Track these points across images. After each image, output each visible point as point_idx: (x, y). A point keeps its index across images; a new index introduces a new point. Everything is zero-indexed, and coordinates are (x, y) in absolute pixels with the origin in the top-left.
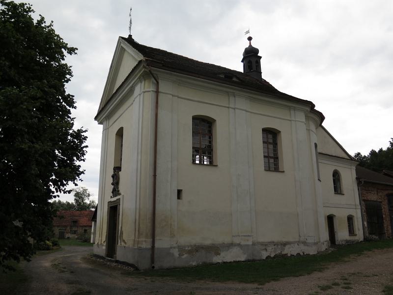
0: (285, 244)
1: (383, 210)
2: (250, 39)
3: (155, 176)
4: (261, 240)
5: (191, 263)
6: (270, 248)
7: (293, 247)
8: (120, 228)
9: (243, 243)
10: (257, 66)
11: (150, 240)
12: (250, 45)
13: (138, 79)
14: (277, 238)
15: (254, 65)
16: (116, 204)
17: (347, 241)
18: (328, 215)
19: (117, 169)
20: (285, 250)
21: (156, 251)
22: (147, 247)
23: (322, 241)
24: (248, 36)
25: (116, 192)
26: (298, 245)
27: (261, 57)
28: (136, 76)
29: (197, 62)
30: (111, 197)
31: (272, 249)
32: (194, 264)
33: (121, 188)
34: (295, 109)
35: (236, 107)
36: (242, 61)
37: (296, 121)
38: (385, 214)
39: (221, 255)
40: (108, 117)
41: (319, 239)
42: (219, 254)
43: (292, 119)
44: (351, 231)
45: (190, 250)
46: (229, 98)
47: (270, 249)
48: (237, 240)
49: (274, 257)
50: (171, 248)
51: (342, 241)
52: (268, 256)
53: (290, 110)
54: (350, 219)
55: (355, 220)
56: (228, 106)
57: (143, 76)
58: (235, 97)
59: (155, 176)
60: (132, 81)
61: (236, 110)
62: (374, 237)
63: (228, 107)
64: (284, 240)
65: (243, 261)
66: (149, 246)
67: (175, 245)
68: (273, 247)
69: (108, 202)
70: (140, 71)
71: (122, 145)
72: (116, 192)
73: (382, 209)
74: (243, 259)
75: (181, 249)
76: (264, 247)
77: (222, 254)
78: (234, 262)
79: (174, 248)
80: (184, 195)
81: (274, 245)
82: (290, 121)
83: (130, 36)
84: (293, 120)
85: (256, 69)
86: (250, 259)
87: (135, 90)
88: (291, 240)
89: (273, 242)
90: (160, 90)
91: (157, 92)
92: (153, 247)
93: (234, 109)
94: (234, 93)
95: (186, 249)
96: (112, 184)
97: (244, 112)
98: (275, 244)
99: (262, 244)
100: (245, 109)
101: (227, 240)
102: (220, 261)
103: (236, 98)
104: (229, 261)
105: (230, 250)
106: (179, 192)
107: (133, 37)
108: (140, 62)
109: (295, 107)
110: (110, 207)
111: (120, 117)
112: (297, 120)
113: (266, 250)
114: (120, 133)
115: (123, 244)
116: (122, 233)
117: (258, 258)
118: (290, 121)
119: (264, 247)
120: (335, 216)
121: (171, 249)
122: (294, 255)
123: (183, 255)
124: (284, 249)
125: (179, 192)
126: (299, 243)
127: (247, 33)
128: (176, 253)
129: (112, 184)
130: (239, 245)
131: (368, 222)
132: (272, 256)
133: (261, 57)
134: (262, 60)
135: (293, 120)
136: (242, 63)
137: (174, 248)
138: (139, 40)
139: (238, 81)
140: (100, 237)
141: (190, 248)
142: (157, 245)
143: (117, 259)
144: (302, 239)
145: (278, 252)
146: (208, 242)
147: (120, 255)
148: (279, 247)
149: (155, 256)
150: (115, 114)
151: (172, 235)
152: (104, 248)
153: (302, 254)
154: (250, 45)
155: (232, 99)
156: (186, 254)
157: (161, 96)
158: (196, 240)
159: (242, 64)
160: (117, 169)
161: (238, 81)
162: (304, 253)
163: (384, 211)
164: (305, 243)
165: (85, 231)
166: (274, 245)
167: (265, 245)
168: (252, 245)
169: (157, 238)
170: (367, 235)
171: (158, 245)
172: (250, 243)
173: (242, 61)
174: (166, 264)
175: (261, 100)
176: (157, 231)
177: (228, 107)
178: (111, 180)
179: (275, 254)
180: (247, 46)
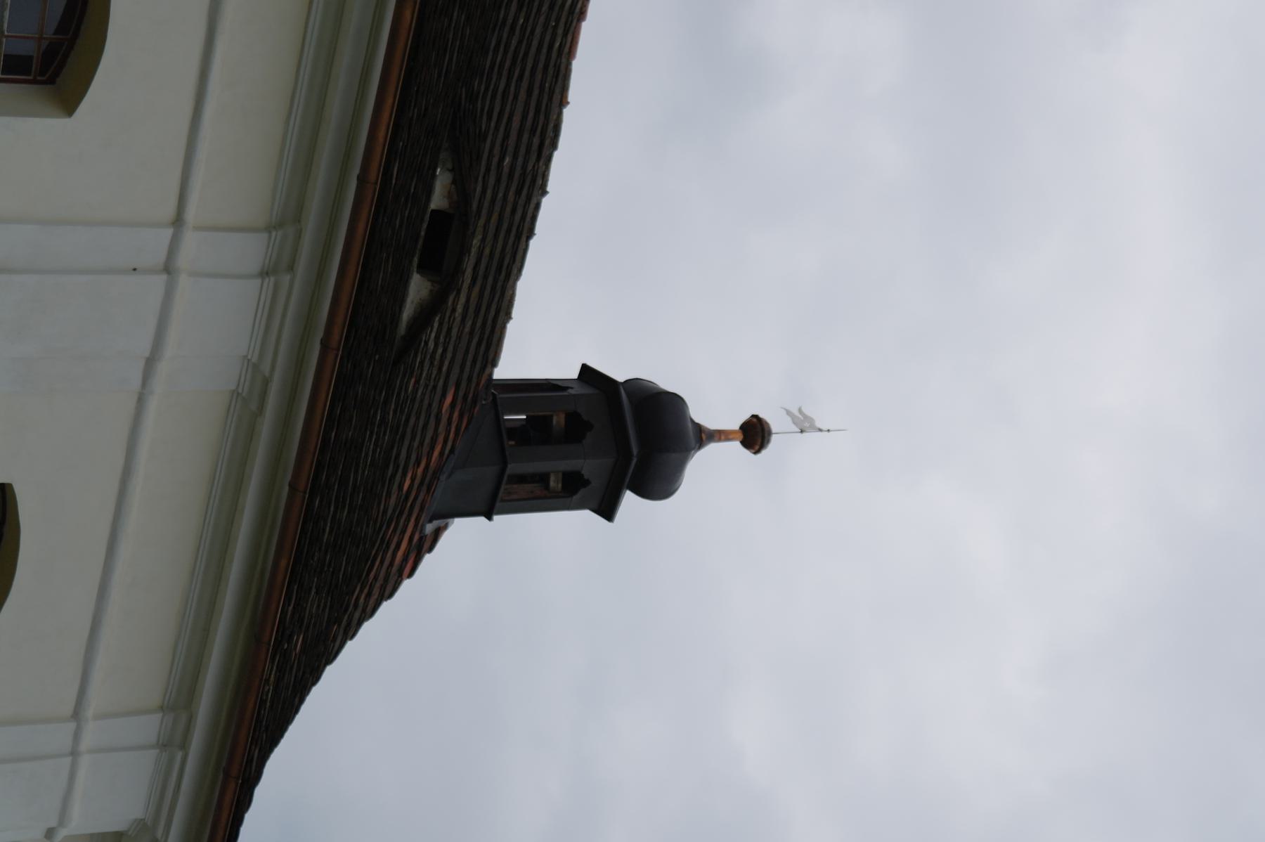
10: (543, 479)
12: (703, 436)
15: (555, 466)
18: (13, 484)
27: (607, 510)
34: (171, 743)
35: (184, 282)
36: (585, 369)
37: (74, 753)
53: (269, 229)
56: (191, 214)
58: (264, 274)
61: (164, 277)
63: (178, 221)
82: (77, 715)
84: (77, 736)
85: (521, 479)
93: (168, 268)
94: (291, 268)
97: (143, 346)
103: (158, 716)
109: (184, 746)
112: (85, 762)
118: (77, 715)
127: (795, 420)
133: (607, 510)
134: (585, 518)
135: (77, 736)
136: (574, 374)
139: (407, 312)
154: (703, 436)
155: (148, 728)
159: (571, 372)
161: (407, 312)
173: (585, 369)
175: (251, 434)
177: (178, 221)
180: (702, 412)
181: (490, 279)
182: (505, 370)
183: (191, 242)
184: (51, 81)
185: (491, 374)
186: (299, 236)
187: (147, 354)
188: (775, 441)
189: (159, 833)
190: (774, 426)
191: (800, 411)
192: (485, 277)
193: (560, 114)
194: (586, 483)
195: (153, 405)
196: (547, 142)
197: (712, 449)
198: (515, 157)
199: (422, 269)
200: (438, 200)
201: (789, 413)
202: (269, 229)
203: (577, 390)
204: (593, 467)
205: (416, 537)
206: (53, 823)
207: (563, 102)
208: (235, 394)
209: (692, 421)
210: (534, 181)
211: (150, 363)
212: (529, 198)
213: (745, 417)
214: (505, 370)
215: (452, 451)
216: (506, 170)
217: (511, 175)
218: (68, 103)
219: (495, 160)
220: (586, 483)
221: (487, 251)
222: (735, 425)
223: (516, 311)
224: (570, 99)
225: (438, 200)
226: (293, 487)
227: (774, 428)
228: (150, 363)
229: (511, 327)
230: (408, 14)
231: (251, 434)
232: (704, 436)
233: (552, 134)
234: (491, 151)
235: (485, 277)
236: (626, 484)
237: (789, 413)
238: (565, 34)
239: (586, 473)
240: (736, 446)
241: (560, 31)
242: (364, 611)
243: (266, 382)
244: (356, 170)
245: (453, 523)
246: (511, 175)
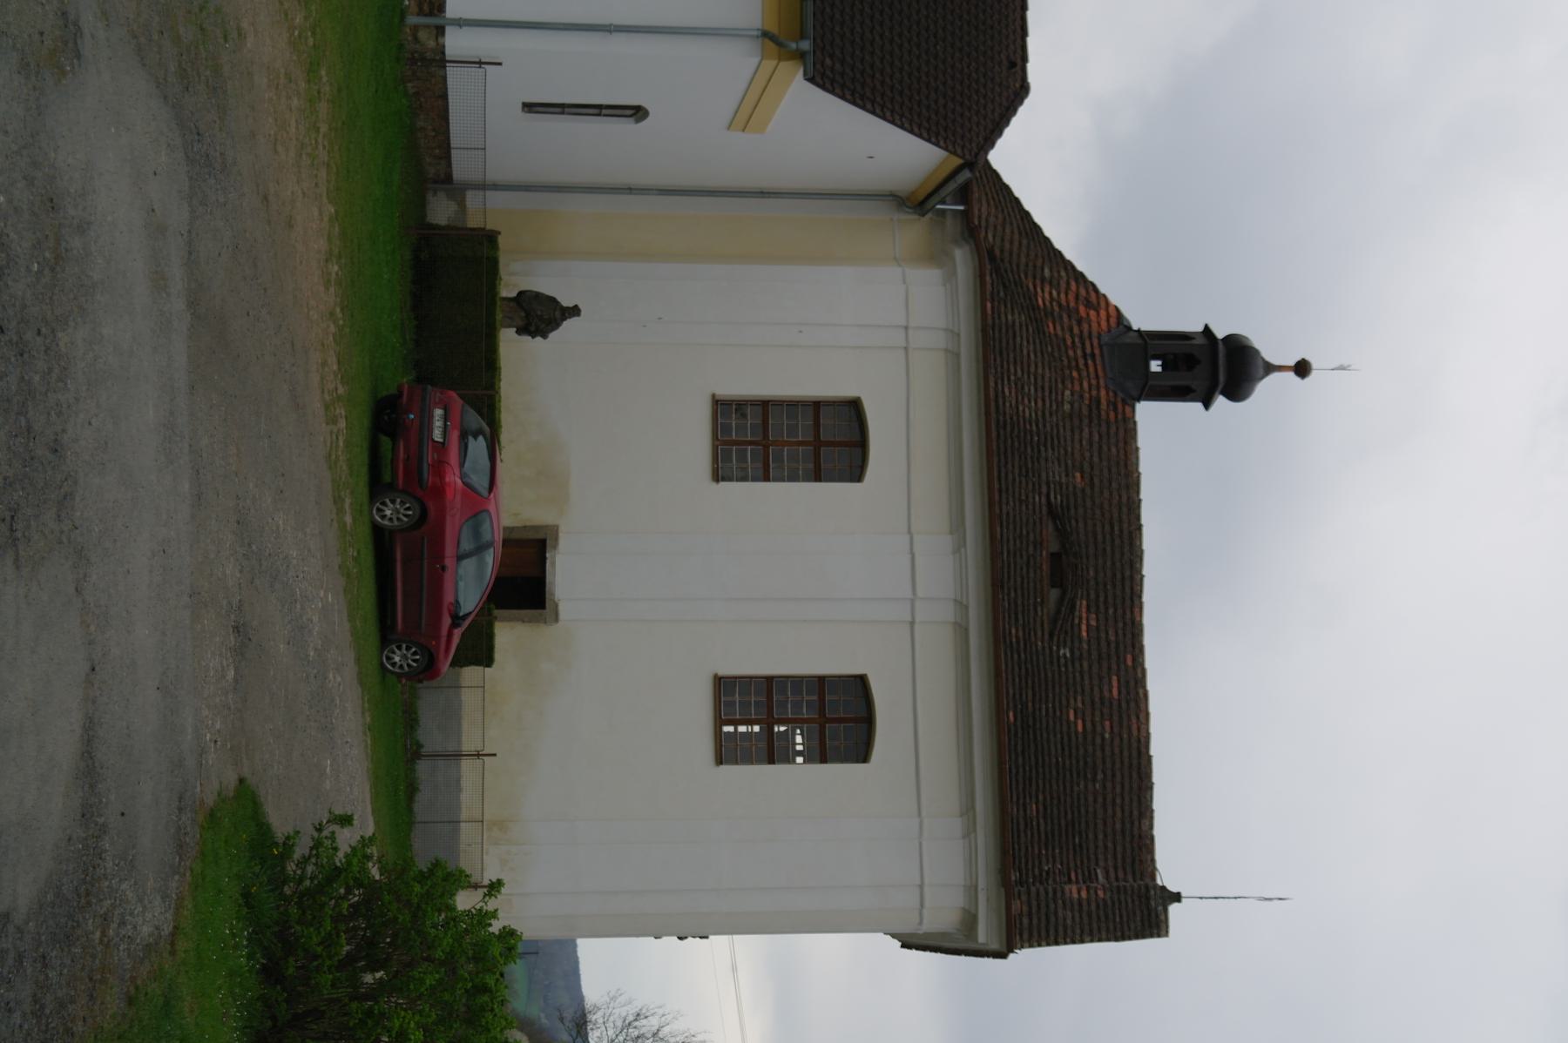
2: (1302, 369)
12: (1270, 368)
27: (1207, 404)
34: (969, 832)
133: (1207, 404)
154: (1270, 368)
155: (956, 825)
188: (1314, 375)
197: (1274, 377)
209: (1263, 359)
222: (1292, 363)
236: (1220, 387)
240: (1291, 375)
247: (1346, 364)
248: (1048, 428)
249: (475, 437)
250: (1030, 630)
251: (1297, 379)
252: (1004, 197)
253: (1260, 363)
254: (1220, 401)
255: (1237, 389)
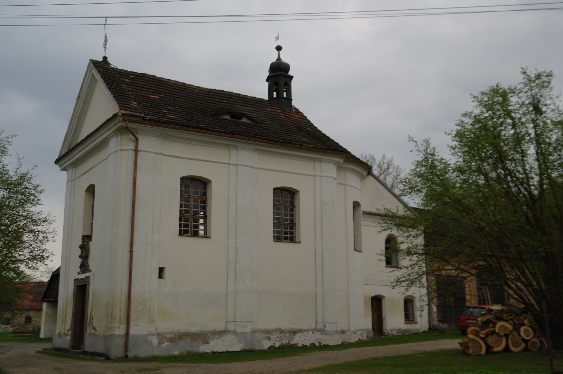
0: (294, 332)
1: (467, 289)
2: (279, 48)
3: (131, 252)
4: (262, 327)
5: (173, 352)
6: (275, 337)
7: (305, 336)
8: (89, 312)
9: (239, 330)
11: (123, 327)
12: (279, 59)
13: (112, 132)
14: (285, 326)
16: (85, 283)
17: (400, 331)
19: (87, 238)
20: (295, 339)
21: (130, 339)
22: (120, 334)
23: (353, 329)
24: (277, 44)
25: (84, 267)
26: (313, 333)
27: (291, 77)
28: (111, 128)
29: (200, 89)
30: (79, 273)
31: (278, 337)
32: (176, 353)
33: (92, 262)
34: (320, 161)
35: (239, 163)
36: (267, 81)
37: (321, 176)
38: (470, 295)
39: (210, 344)
40: (76, 164)
41: (349, 326)
42: (208, 343)
43: (317, 174)
44: (409, 316)
45: (172, 337)
46: (230, 152)
47: (274, 337)
48: (231, 327)
49: (279, 348)
50: (149, 335)
51: (392, 330)
52: (272, 346)
53: (230, 149)
54: (408, 303)
55: (417, 304)
56: (228, 162)
57: (119, 130)
58: (237, 150)
59: (131, 252)
60: (105, 132)
61: (238, 166)
62: (445, 326)
63: (229, 164)
64: (295, 327)
65: (238, 352)
66: (122, 332)
67: (154, 332)
68: (279, 335)
69: (75, 280)
70: (115, 125)
71: (93, 205)
72: (84, 267)
73: (465, 288)
74: (238, 349)
75: (161, 336)
76: (267, 335)
77: (212, 343)
78: (227, 352)
79: (153, 335)
80: (166, 273)
81: (280, 334)
82: (314, 176)
83: (105, 58)
86: (247, 348)
87: (109, 142)
88: (304, 327)
89: (280, 329)
90: (140, 148)
91: (136, 151)
92: (127, 333)
93: (237, 165)
94: (236, 146)
95: (168, 336)
96: (80, 257)
97: (250, 169)
98: (281, 331)
99: (264, 331)
100: (250, 164)
101: (220, 327)
102: (209, 351)
104: (220, 351)
105: (222, 338)
106: (161, 270)
107: (109, 60)
108: (115, 116)
109: (321, 159)
110: (77, 286)
111: (91, 169)
112: (323, 174)
113: (269, 339)
114: (91, 190)
115: (93, 331)
116: (92, 318)
117: (258, 348)
118: (314, 176)
119: (267, 335)
120: (384, 297)
121: (149, 337)
122: (306, 346)
123: (163, 343)
124: (294, 338)
125: (161, 270)
126: (314, 331)
128: (155, 340)
129: (80, 257)
130: (234, 332)
131: (438, 306)
132: (277, 345)
133: (291, 77)
134: (293, 82)
135: (318, 176)
136: (267, 83)
137: (153, 335)
138: (117, 62)
139: (249, 121)
140: (62, 324)
141: (172, 336)
142: (132, 332)
143: (85, 350)
144: (320, 326)
145: (285, 341)
146: (195, 329)
147: (89, 345)
148: (287, 335)
149: (130, 344)
150: (84, 162)
151: (151, 321)
152: (69, 338)
153: (318, 344)
154: (279, 59)
155: (318, 164)
156: (167, 342)
157: (141, 156)
158: (181, 326)
160: (87, 238)
162: (320, 343)
163: (470, 290)
164: (322, 331)
165: (28, 319)
166: (280, 334)
167: (268, 333)
168: (251, 332)
169: (132, 323)
170: (436, 323)
171: (133, 331)
172: (248, 330)
173: (267, 81)
174: (143, 352)
176: (133, 315)
178: (79, 252)
179: (280, 344)
180: (274, 59)
181: (247, 103)
182: (266, 97)
183: (232, 162)
184: (207, 183)
185: (266, 100)
186: (231, 145)
187: (251, 168)
188: (280, 44)
189: (336, 162)
190: (277, 45)
191: (276, 38)
192: (246, 104)
193: (217, 90)
194: (286, 82)
195: (260, 166)
196: (223, 93)
197: (281, 57)
198: (224, 100)
199: (241, 119)
200: (228, 117)
201: (276, 41)
202: (230, 149)
203: (270, 82)
204: (283, 81)
205: (295, 113)
206: (333, 179)
207: (215, 90)
208: (259, 153)
209: (276, 61)
210: (229, 95)
211: (253, 167)
212: (233, 96)
213: (275, 50)
214: (266, 97)
215: (279, 107)
216: (227, 102)
217: (228, 100)
218: (210, 181)
219: (224, 104)
220: (286, 82)
221: (241, 104)
222: (277, 52)
223: (254, 96)
224: (215, 88)
225: (228, 117)
226: (274, 144)
227: (278, 45)
228: (253, 167)
229: (257, 97)
230: (192, 130)
231: (266, 151)
232: (279, 58)
233: (221, 92)
234: (222, 105)
235: (246, 104)
236: (286, 74)
237: (276, 41)
238: (203, 91)
239: (284, 82)
240: (281, 52)
241: (202, 92)
242: (308, 123)
243: (256, 149)
244: (219, 137)
245: (294, 106)
246: (228, 100)
247: (473, 102)
248: (239, 106)
249: (426, 198)
250: (266, 119)
251: (282, 50)
252: (268, 120)
253: (278, 61)
254: (290, 73)
255: (286, 68)
